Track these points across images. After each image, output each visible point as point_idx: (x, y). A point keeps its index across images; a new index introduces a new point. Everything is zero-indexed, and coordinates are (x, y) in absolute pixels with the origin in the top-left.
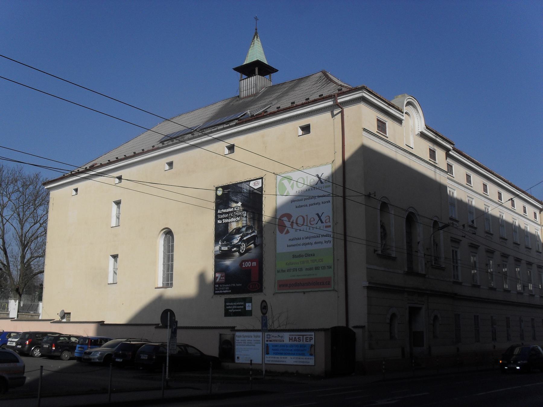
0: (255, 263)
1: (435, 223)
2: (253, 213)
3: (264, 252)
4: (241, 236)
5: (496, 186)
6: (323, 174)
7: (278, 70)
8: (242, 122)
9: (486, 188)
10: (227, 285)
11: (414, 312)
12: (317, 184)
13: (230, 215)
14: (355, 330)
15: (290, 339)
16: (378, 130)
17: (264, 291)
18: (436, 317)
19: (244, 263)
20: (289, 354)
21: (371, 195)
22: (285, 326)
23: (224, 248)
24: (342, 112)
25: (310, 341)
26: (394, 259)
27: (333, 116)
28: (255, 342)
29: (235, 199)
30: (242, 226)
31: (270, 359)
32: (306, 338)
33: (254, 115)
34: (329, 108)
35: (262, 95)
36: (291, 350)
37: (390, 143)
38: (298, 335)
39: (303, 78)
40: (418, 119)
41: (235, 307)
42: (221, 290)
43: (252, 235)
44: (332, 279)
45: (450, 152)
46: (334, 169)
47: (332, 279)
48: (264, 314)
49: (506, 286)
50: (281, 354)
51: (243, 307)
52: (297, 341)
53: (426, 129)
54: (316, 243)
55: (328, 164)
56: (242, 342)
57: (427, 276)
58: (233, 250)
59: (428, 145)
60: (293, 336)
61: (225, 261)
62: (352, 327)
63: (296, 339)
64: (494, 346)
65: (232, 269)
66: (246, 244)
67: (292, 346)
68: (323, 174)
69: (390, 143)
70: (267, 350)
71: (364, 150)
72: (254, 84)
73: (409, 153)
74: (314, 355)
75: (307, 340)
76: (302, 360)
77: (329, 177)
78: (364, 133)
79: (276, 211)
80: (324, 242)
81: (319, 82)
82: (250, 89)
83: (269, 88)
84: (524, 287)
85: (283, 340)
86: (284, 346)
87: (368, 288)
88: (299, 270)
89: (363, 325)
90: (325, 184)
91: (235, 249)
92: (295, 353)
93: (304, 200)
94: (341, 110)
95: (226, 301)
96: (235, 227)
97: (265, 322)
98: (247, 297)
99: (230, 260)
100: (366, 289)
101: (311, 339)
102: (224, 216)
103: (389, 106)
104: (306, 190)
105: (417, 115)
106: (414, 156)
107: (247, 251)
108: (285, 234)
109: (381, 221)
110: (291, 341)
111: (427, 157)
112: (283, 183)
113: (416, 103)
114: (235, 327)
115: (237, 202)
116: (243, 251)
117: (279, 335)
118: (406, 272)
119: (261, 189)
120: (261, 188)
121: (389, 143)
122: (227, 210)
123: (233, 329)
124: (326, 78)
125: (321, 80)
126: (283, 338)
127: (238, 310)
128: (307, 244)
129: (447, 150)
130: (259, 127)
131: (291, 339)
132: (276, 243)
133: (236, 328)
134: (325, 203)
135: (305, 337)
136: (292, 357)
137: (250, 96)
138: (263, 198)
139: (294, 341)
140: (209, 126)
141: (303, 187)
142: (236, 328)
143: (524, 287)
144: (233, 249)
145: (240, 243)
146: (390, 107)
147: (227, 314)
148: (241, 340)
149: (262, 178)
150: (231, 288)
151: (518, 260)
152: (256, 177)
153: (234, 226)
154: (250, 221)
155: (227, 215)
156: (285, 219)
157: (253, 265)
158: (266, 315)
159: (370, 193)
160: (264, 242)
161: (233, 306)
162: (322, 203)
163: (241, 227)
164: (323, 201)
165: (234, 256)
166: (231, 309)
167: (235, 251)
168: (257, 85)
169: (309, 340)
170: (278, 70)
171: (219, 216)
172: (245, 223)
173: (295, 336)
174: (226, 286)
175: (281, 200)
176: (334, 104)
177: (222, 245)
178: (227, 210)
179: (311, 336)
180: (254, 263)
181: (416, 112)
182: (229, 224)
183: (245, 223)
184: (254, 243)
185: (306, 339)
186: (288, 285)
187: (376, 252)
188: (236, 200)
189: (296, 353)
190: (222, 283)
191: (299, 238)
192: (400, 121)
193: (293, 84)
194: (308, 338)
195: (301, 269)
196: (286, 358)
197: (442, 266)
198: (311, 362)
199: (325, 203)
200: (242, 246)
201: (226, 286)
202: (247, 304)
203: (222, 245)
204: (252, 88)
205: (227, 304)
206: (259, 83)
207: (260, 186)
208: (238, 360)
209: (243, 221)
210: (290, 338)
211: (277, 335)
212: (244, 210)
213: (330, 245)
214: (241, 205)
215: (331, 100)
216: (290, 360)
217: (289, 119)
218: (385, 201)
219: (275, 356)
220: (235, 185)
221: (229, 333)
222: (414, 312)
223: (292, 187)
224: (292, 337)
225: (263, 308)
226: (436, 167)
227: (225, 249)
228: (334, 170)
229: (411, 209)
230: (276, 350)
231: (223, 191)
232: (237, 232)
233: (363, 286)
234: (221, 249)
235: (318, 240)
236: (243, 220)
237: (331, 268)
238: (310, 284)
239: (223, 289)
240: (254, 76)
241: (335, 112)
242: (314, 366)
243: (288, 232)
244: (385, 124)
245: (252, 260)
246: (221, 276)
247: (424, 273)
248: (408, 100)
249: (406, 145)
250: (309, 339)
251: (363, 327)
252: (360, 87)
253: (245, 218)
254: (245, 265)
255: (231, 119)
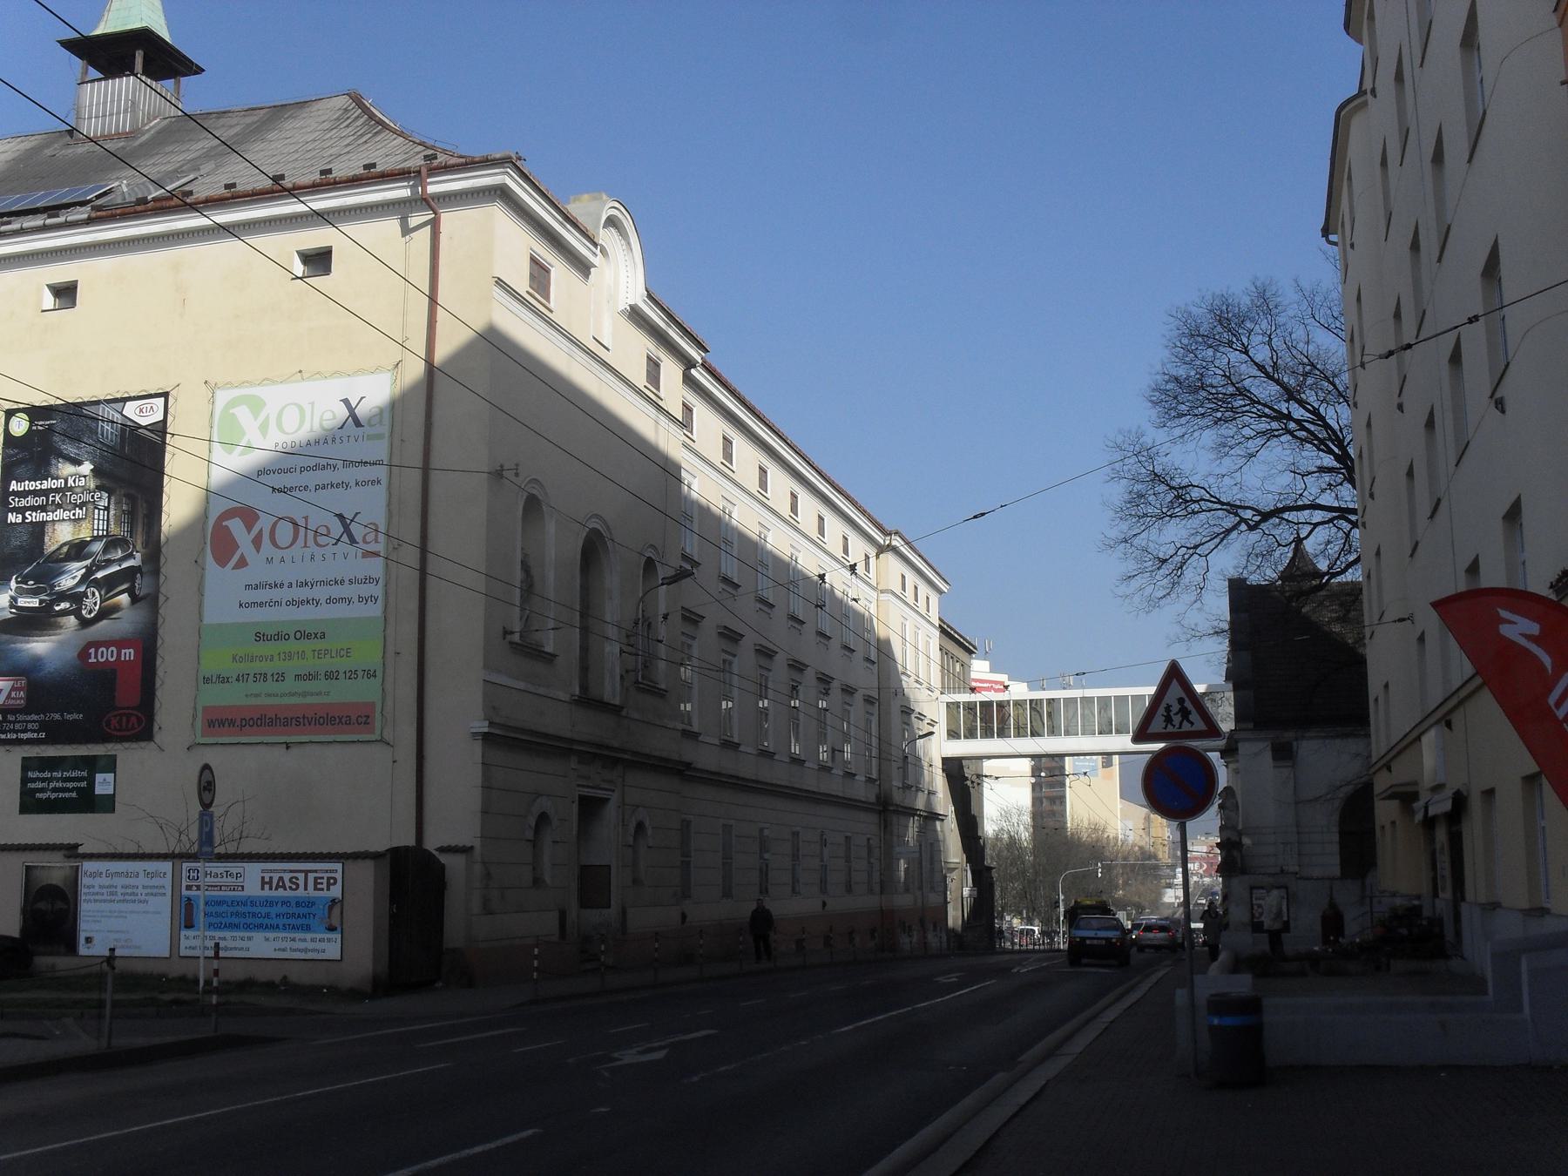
0: (132, 651)
1: (650, 565)
2: (132, 499)
3: (160, 621)
4: (86, 567)
5: (788, 475)
6: (362, 398)
7: (203, 70)
8: (106, 214)
9: (764, 479)
10: (35, 717)
11: (590, 808)
12: (341, 428)
13: (51, 499)
14: (443, 858)
15: (263, 883)
16: (531, 287)
17: (157, 738)
18: (640, 826)
19: (92, 651)
20: (260, 927)
21: (504, 473)
22: (235, 844)
23: (28, 600)
24: (435, 224)
25: (328, 889)
26: (550, 658)
27: (406, 231)
28: (149, 891)
29: (70, 449)
30: (93, 536)
31: (194, 943)
32: (316, 879)
33: (149, 198)
34: (397, 206)
35: (153, 138)
36: (268, 915)
37: (558, 330)
38: (291, 871)
39: (286, 105)
40: (628, 269)
41: (60, 785)
42: (10, 731)
43: (122, 567)
44: (378, 709)
45: (693, 371)
46: (398, 387)
47: (378, 709)
48: (206, 806)
49: (796, 749)
50: (235, 927)
51: (84, 784)
52: (285, 889)
53: (646, 299)
54: (330, 601)
55: (381, 372)
56: (104, 891)
57: (624, 713)
58: (57, 608)
59: (643, 345)
60: (272, 875)
61: (28, 642)
62: (436, 850)
63: (283, 882)
64: (684, 917)
65: (51, 667)
66: (103, 593)
67: (270, 902)
68: (362, 398)
69: (558, 330)
70: (185, 915)
71: (492, 342)
72: (127, 100)
73: (601, 363)
74: (339, 929)
75: (319, 886)
76: (302, 945)
77: (381, 411)
78: (498, 292)
79: (209, 494)
80: (355, 599)
81: (345, 124)
82: (111, 114)
83: (174, 119)
84: (835, 752)
85: (243, 887)
86: (244, 904)
87: (487, 738)
88: (276, 677)
89: (470, 845)
90: (367, 430)
91: (64, 605)
92: (277, 925)
93: (298, 470)
94: (433, 216)
95: (27, 764)
96: (68, 538)
97: (207, 830)
98: (101, 756)
99: (46, 638)
100: (480, 743)
101: (332, 881)
102: (31, 501)
103: (565, 223)
104: (309, 444)
105: (626, 258)
106: (611, 371)
107: (104, 614)
108: (233, 568)
109: (522, 549)
110: (267, 887)
111: (640, 379)
112: (233, 414)
113: (628, 224)
114: (76, 846)
115: (77, 462)
116: (90, 612)
117: (228, 869)
118: (576, 698)
119: (161, 428)
120: (161, 424)
121: (554, 327)
122: (41, 484)
123: (71, 851)
124: (360, 110)
125: (348, 118)
126: (241, 879)
127: (67, 795)
128: (302, 602)
129: (689, 364)
130: (166, 239)
131: (267, 883)
132: (202, 595)
133: (81, 850)
134: (365, 483)
135: (311, 876)
136: (271, 935)
137: (113, 135)
138: (168, 457)
139: (276, 889)
140: (7, 210)
141: (296, 434)
142: (81, 850)
143: (835, 752)
144: (59, 605)
145: (82, 589)
146: (568, 226)
147: (31, 804)
148: (100, 887)
149: (166, 395)
150: (43, 726)
151: (825, 680)
152: (146, 391)
153: (62, 533)
154: (119, 522)
155: (40, 500)
156: (236, 526)
157: (127, 659)
158: (211, 809)
159: (502, 466)
160: (163, 590)
161: (49, 780)
162: (357, 484)
163: (88, 539)
164: (360, 479)
165: (61, 627)
166: (42, 790)
167: (64, 613)
168: (139, 107)
169: (325, 886)
170: (203, 70)
171: (12, 499)
172: (101, 528)
173: (282, 875)
174: (29, 718)
175: (230, 463)
176: (414, 197)
177: (20, 592)
178: (41, 484)
179: (333, 875)
180: (127, 651)
181: (624, 247)
182: (49, 529)
183: (101, 528)
184: (131, 592)
185: (316, 883)
186: (238, 723)
187: (509, 637)
188: (76, 454)
189: (284, 925)
190: (14, 711)
191: (279, 582)
192: (583, 267)
193: (256, 118)
194: (323, 878)
195: (280, 677)
196: (250, 939)
197: (659, 687)
198: (330, 947)
199: (365, 483)
200: (87, 598)
201: (29, 718)
202: (99, 777)
203: (20, 592)
204: (118, 113)
205: (30, 774)
206: (144, 106)
207: (159, 417)
208: (88, 948)
209: (96, 522)
210: (263, 878)
211: (222, 870)
212: (99, 488)
213: (376, 610)
214: (92, 470)
215: (406, 184)
216: (261, 945)
217: (288, 221)
218: (534, 492)
219: (292, 935)
220: (78, 406)
221: (58, 865)
222: (590, 808)
223: (264, 429)
224: (271, 878)
225: (205, 789)
226: (659, 408)
227: (31, 605)
228: (397, 390)
229: (594, 520)
230: (218, 915)
231: (31, 422)
232: (73, 553)
233: (472, 733)
234: (16, 603)
235: (336, 591)
236: (96, 517)
237: (375, 676)
238: (306, 720)
239: (17, 726)
240: (129, 75)
241: (414, 221)
242: (166, 958)
243: (242, 563)
244: (547, 271)
245: (120, 644)
246: (13, 689)
247: (617, 701)
248: (615, 212)
249: (594, 338)
250: (325, 881)
251: (466, 850)
252: (498, 156)
253: (101, 512)
254: (96, 657)
255: (65, 201)
